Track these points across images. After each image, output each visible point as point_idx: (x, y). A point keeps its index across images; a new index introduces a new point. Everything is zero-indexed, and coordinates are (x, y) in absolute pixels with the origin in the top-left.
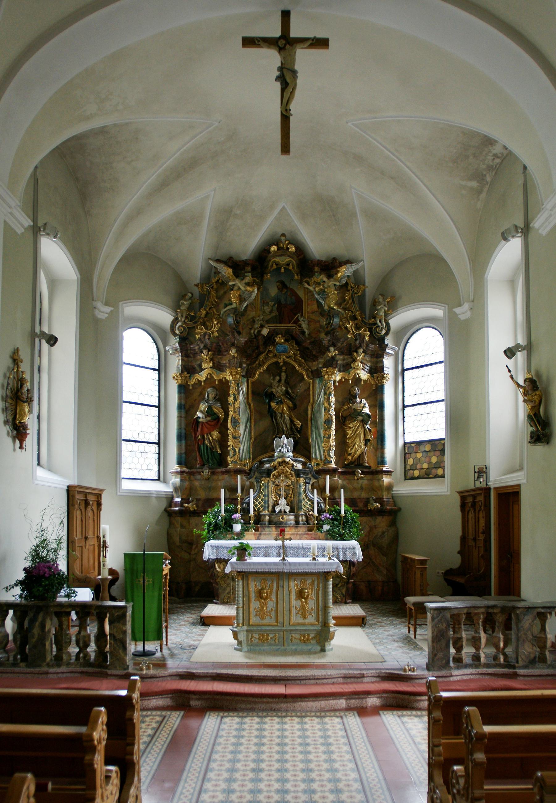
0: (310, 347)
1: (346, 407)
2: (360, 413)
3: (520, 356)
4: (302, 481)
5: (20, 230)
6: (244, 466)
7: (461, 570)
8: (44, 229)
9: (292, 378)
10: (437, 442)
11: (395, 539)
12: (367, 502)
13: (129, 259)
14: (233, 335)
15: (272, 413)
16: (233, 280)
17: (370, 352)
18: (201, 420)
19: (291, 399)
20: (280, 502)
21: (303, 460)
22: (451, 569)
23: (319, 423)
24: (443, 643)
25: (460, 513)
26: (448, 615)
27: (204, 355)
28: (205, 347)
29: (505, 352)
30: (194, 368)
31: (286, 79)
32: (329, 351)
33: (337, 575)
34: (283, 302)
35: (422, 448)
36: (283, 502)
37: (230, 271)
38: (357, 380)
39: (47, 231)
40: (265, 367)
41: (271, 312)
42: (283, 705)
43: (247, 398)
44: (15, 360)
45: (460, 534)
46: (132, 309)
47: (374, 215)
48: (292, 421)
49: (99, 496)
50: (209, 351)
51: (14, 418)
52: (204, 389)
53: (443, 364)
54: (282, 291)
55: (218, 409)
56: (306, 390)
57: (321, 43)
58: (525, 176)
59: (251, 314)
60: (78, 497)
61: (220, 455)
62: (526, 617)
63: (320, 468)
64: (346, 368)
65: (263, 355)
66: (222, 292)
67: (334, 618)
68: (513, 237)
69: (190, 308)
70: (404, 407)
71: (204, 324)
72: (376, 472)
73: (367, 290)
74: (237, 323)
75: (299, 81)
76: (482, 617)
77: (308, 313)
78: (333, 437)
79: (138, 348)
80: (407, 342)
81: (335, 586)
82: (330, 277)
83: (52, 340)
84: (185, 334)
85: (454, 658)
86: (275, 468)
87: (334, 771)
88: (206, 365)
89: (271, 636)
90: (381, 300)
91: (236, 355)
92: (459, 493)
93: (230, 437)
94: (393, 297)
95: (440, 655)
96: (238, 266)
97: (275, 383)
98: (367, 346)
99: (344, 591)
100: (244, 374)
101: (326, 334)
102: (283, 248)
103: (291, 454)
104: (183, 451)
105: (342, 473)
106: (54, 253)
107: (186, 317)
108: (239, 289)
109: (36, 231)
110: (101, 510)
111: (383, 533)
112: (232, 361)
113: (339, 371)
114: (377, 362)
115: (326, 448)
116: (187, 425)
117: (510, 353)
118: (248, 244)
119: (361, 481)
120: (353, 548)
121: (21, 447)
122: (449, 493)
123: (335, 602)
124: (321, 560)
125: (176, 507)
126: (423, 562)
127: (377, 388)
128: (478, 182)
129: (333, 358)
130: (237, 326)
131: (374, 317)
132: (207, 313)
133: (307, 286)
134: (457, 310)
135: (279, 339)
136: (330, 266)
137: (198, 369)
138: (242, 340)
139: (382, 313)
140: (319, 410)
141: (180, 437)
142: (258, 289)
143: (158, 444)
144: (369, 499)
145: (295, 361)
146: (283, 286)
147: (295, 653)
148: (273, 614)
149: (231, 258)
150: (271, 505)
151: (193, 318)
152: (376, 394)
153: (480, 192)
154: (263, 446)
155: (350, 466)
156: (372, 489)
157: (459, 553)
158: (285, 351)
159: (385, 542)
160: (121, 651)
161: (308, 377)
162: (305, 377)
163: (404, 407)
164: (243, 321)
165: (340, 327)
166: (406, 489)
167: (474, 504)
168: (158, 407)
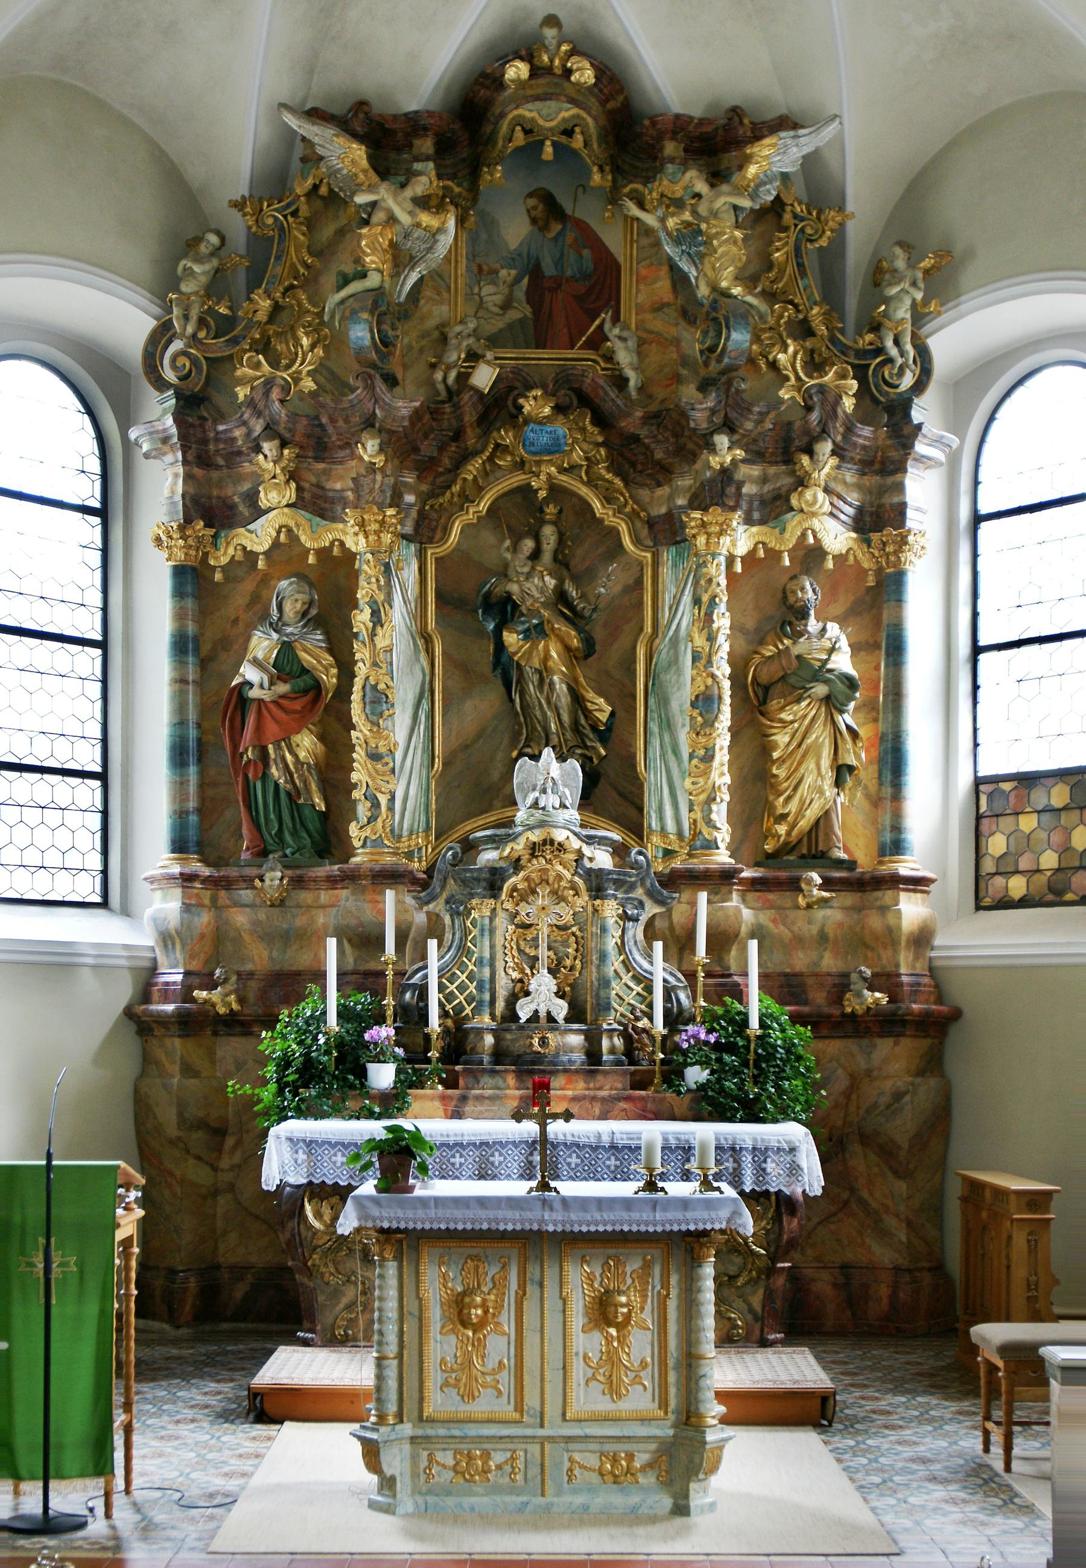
2: (820, 673)
4: (610, 910)
9: (580, 545)
12: (841, 986)
15: (506, 671)
19: (575, 618)
27: (269, 460)
33: (732, 1245)
36: (543, 984)
38: (811, 556)
59: (436, 312)
64: (773, 508)
69: (216, 287)
71: (264, 347)
81: (723, 1282)
82: (717, 177)
94: (945, 253)
96: (386, 137)
115: (694, 790)
118: (421, 59)
120: (791, 1150)
123: (727, 1340)
126: (1037, 1201)
136: (718, 141)
138: (403, 406)
141: (179, 755)
146: (549, 210)
151: (224, 326)
154: (474, 788)
155: (785, 861)
156: (859, 942)
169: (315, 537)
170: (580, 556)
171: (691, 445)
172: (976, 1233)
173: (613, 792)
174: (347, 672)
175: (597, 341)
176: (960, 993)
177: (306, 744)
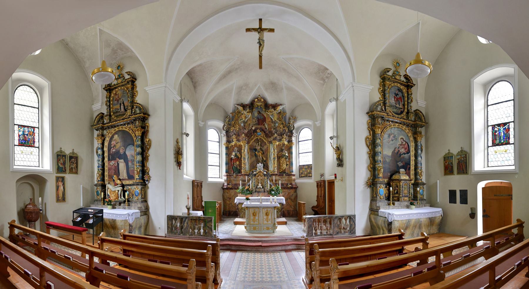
2: (285, 156)
3: (335, 139)
4: (266, 178)
5: (177, 101)
7: (317, 207)
9: (263, 144)
11: (296, 197)
12: (287, 184)
15: (256, 155)
19: (262, 150)
27: (234, 137)
31: (261, 43)
33: (278, 208)
36: (260, 185)
38: (284, 144)
42: (261, 249)
43: (248, 150)
44: (177, 142)
46: (210, 123)
47: (289, 89)
49: (201, 183)
57: (272, 30)
59: (249, 122)
60: (196, 184)
64: (280, 140)
69: (229, 121)
71: (233, 126)
72: (290, 175)
74: (244, 125)
75: (265, 43)
81: (277, 212)
82: (275, 110)
83: (187, 135)
87: (277, 268)
94: (295, 117)
95: (310, 232)
96: (244, 106)
106: (186, 106)
109: (182, 101)
115: (273, 167)
117: (331, 138)
118: (247, 100)
120: (282, 199)
123: (277, 217)
126: (304, 204)
135: (258, 131)
136: (275, 106)
138: (246, 131)
141: (226, 164)
146: (259, 113)
151: (230, 125)
153: (324, 85)
154: (253, 167)
155: (282, 173)
156: (289, 180)
159: (293, 198)
164: (246, 125)
166: (299, 181)
169: (238, 143)
170: (262, 145)
171: (273, 134)
172: (299, 207)
173: (266, 167)
174: (241, 156)
175: (264, 125)
176: (298, 185)
177: (238, 163)
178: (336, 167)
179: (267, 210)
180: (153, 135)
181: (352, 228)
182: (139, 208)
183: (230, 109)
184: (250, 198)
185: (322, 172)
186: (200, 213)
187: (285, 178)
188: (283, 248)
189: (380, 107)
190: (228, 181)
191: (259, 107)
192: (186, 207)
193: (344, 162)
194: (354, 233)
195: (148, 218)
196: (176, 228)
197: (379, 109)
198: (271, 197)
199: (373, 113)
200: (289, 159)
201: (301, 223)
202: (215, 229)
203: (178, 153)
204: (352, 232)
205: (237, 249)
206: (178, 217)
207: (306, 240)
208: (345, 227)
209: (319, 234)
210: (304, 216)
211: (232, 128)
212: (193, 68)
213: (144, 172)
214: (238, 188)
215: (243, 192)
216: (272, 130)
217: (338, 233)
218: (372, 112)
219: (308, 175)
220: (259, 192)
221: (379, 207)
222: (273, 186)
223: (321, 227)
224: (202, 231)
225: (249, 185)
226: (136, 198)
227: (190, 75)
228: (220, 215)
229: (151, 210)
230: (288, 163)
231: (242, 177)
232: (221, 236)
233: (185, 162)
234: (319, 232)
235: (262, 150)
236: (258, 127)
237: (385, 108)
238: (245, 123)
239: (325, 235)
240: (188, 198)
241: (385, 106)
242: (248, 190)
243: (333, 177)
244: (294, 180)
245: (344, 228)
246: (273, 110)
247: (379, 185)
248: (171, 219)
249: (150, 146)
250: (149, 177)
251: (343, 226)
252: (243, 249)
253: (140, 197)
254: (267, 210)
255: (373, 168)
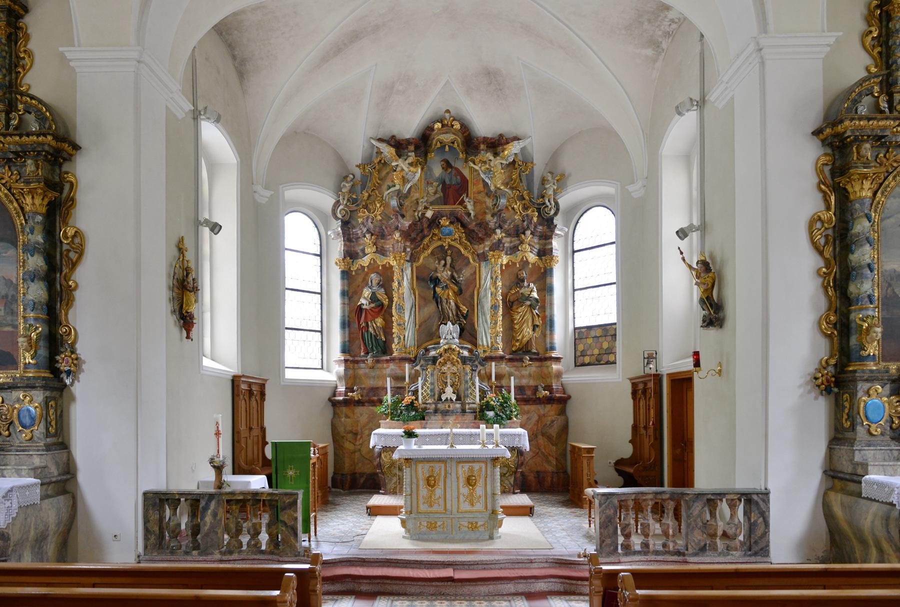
0: (476, 229)
1: (513, 292)
2: (528, 298)
3: (695, 236)
4: (468, 368)
5: (180, 115)
6: (409, 353)
8: (205, 113)
9: (457, 261)
10: (608, 327)
11: (565, 429)
12: (535, 389)
13: (288, 140)
14: (397, 218)
15: (436, 299)
16: (396, 161)
17: (538, 234)
18: (364, 307)
19: (457, 283)
20: (446, 390)
21: (469, 346)
22: (622, 459)
23: (486, 308)
24: (611, 529)
25: (632, 401)
26: (616, 502)
27: (368, 239)
28: (368, 231)
29: (677, 232)
30: (357, 253)
32: (495, 233)
33: (505, 464)
34: (448, 182)
35: (593, 333)
36: (449, 390)
37: (393, 150)
39: (208, 116)
40: (429, 251)
41: (435, 193)
42: (451, 590)
44: (181, 250)
45: (632, 422)
46: (292, 193)
48: (458, 307)
49: (262, 386)
50: (372, 235)
51: (181, 307)
52: (367, 274)
53: (614, 245)
54: (446, 170)
55: (381, 294)
56: (471, 275)
58: (702, 45)
60: (244, 387)
61: (385, 342)
62: (696, 504)
63: (487, 354)
64: (514, 249)
65: (428, 238)
66: (384, 173)
67: (502, 507)
68: (688, 110)
70: (574, 290)
72: (544, 358)
73: (535, 167)
76: (650, 503)
77: (474, 193)
78: (500, 323)
79: (300, 234)
80: (577, 222)
81: (502, 475)
82: (496, 154)
83: (216, 228)
84: (347, 218)
85: (622, 545)
86: (441, 355)
88: (369, 250)
89: (439, 524)
90: (550, 178)
91: (400, 239)
92: (631, 379)
93: (395, 324)
94: (563, 175)
95: (608, 541)
96: (399, 146)
97: (441, 268)
98: (535, 227)
99: (512, 480)
100: (408, 258)
101: (493, 216)
102: (447, 125)
103: (457, 340)
104: (347, 339)
105: (510, 360)
106: (212, 135)
107: (348, 200)
108: (403, 170)
109: (196, 116)
110: (264, 400)
111: (553, 421)
112: (396, 245)
113: (506, 254)
114: (545, 244)
115: (490, 333)
116: (350, 312)
117: (682, 234)
118: (409, 126)
119: (528, 368)
120: (520, 436)
121: (188, 337)
122: (620, 380)
123: (504, 492)
124: (490, 447)
125: (340, 396)
126: (590, 451)
127: (545, 271)
128: (653, 49)
129: (500, 241)
130: (400, 209)
131: (543, 197)
132: (370, 196)
133: (472, 165)
134: (631, 188)
136: (496, 144)
137: (361, 254)
138: (406, 223)
139: (551, 192)
140: (486, 295)
141: (345, 325)
142: (422, 169)
143: (321, 332)
144: (537, 386)
145: (460, 244)
146: (447, 165)
147: (462, 541)
148: (441, 502)
149: (393, 137)
150: (437, 393)
151: (354, 201)
152: (543, 277)
153: (655, 61)
154: (428, 334)
157: (630, 442)
158: (450, 234)
159: (554, 431)
160: (292, 538)
161: (474, 260)
162: (471, 261)
163: (574, 290)
165: (507, 208)
167: (645, 391)
168: (321, 294)
169: (381, 261)
173: (468, 333)
174: (391, 300)
175: (462, 202)
176: (570, 391)
177: (379, 321)
178: (699, 329)
179: (471, 470)
180: (90, 216)
181: (754, 538)
182: (36, 471)
183: (356, 152)
184: (418, 431)
185: (650, 348)
186: (258, 482)
187: (530, 368)
188: (522, 587)
189: (867, 100)
190: (351, 379)
191: (448, 147)
192: (212, 461)
193: (729, 310)
194: (764, 551)
195: (74, 506)
196: (176, 532)
197: (863, 110)
198: (483, 429)
199: (840, 129)
200: (543, 308)
201: (578, 511)
202: (307, 530)
203: (184, 287)
204: (756, 548)
205: (377, 588)
206: (182, 494)
207: (592, 559)
208: (730, 532)
209: (638, 548)
210: (589, 491)
211: (362, 214)
212: (235, 14)
213: (55, 342)
214: (380, 402)
215: (395, 414)
216: (488, 217)
217: (703, 549)
218: (834, 124)
219: (604, 359)
220: (445, 413)
221: (865, 466)
222: (490, 395)
223: (646, 527)
224: (264, 537)
225: (415, 392)
226: (25, 435)
227: (225, 32)
228: (322, 485)
229: (82, 478)
230: (538, 322)
231: (392, 366)
232: (328, 551)
233: (207, 316)
234: (636, 541)
235: (457, 283)
236: (449, 210)
237: (890, 102)
238: (400, 195)
239: (657, 553)
240: (218, 434)
241: (890, 96)
242: (411, 406)
243: (687, 364)
244: (559, 375)
245: (725, 535)
246: (489, 156)
247: (862, 387)
248: (157, 502)
249: (81, 255)
250: (77, 362)
251: (721, 526)
252: (395, 588)
253: (39, 430)
254: (471, 470)
255: (841, 326)
